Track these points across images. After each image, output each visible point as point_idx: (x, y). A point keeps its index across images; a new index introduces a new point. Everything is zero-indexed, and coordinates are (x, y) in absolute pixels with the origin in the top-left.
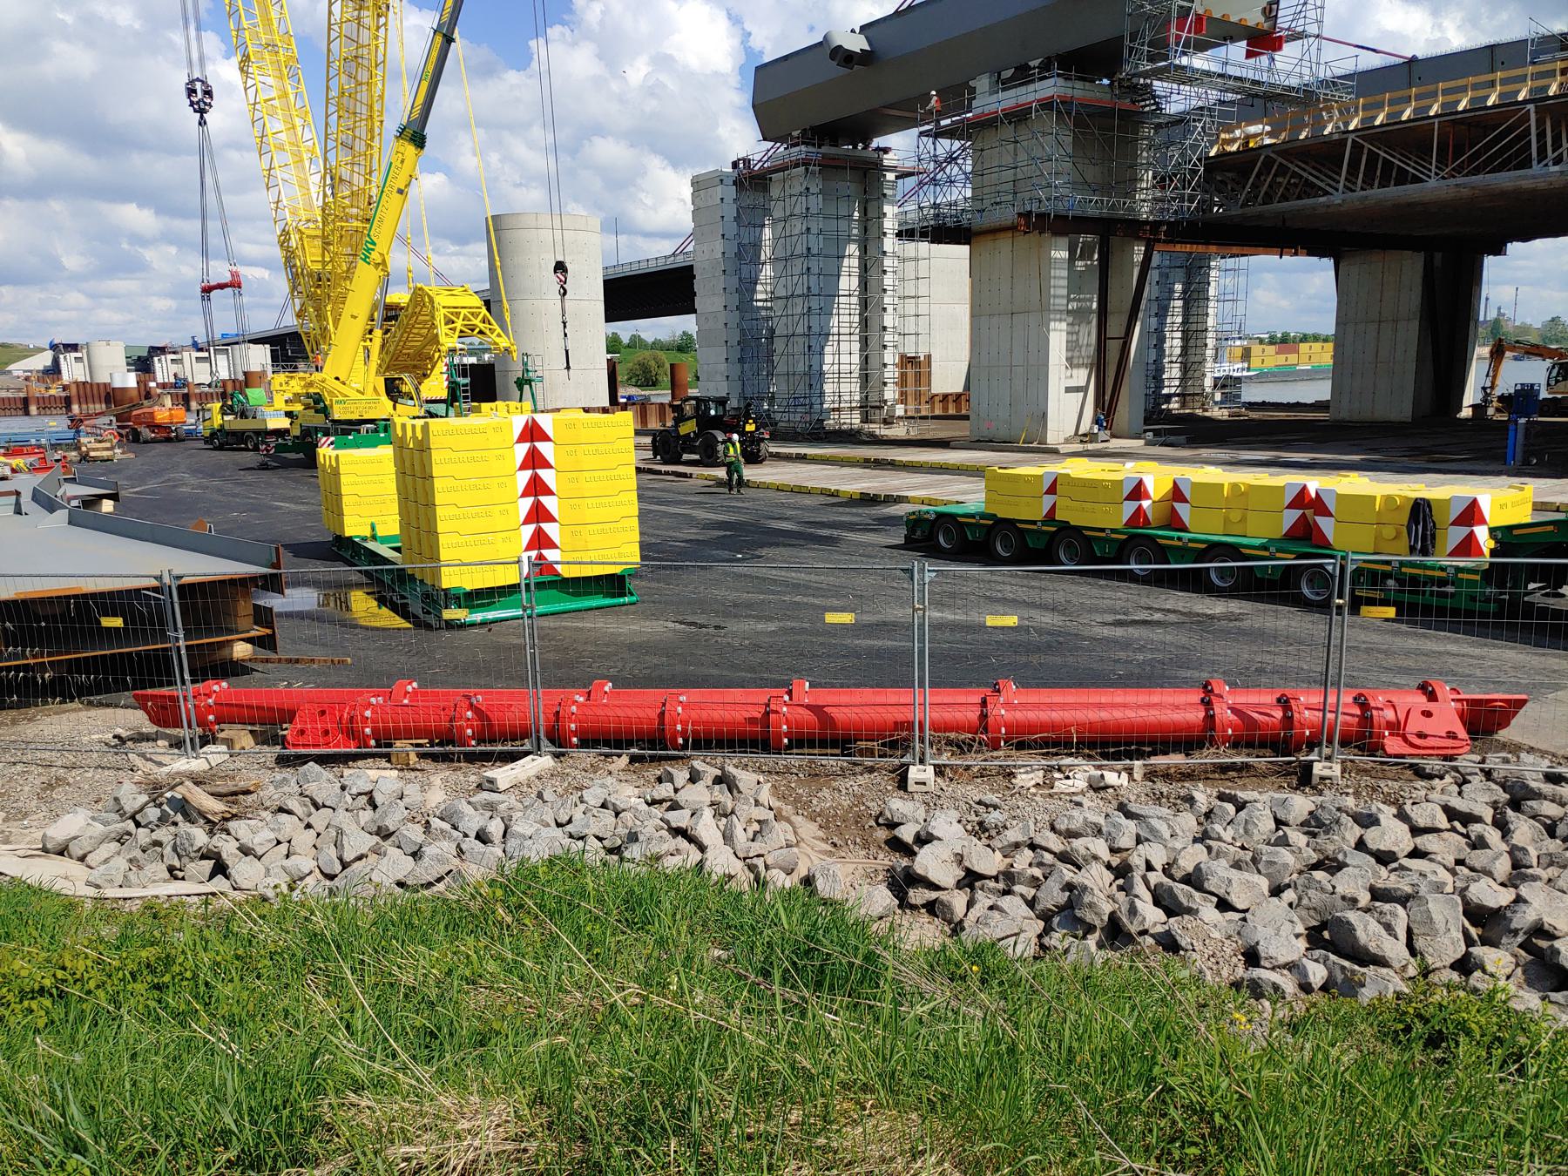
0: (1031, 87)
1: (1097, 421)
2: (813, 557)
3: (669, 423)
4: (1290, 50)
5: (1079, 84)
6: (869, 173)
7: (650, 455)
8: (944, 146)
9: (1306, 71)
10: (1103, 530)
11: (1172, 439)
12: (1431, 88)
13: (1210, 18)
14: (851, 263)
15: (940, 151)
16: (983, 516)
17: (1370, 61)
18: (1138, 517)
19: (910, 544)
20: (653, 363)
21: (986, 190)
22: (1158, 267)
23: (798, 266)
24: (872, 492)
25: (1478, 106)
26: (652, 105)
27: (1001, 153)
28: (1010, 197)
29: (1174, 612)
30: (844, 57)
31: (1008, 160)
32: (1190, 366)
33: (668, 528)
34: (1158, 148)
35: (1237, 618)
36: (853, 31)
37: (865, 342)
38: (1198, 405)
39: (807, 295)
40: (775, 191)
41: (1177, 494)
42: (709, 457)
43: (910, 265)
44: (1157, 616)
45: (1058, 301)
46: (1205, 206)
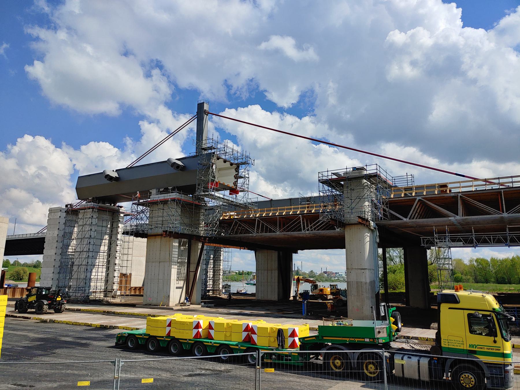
0: (169, 195)
1: (186, 299)
2: (77, 352)
3: (24, 296)
4: (241, 194)
5: (183, 195)
6: (115, 214)
7: (13, 309)
8: (141, 208)
9: (245, 200)
10: (186, 340)
11: (210, 305)
12: (276, 208)
13: (220, 183)
14: (106, 241)
15: (139, 209)
16: (145, 335)
17: (261, 199)
18: (198, 335)
19: (117, 346)
20: (22, 272)
21: (153, 223)
22: (206, 250)
23: (86, 241)
24: (105, 325)
25: (287, 214)
26: (37, 181)
27: (158, 212)
28: (161, 226)
29: (209, 370)
30: (109, 178)
31: (160, 214)
32: (215, 282)
33: (16, 341)
34: (206, 216)
35: (228, 371)
36: (113, 171)
37: (108, 269)
38: (218, 293)
39: (88, 251)
40: (80, 216)
41: (210, 327)
42: (39, 310)
43: (126, 244)
44: (203, 372)
45: (175, 259)
46: (219, 233)
